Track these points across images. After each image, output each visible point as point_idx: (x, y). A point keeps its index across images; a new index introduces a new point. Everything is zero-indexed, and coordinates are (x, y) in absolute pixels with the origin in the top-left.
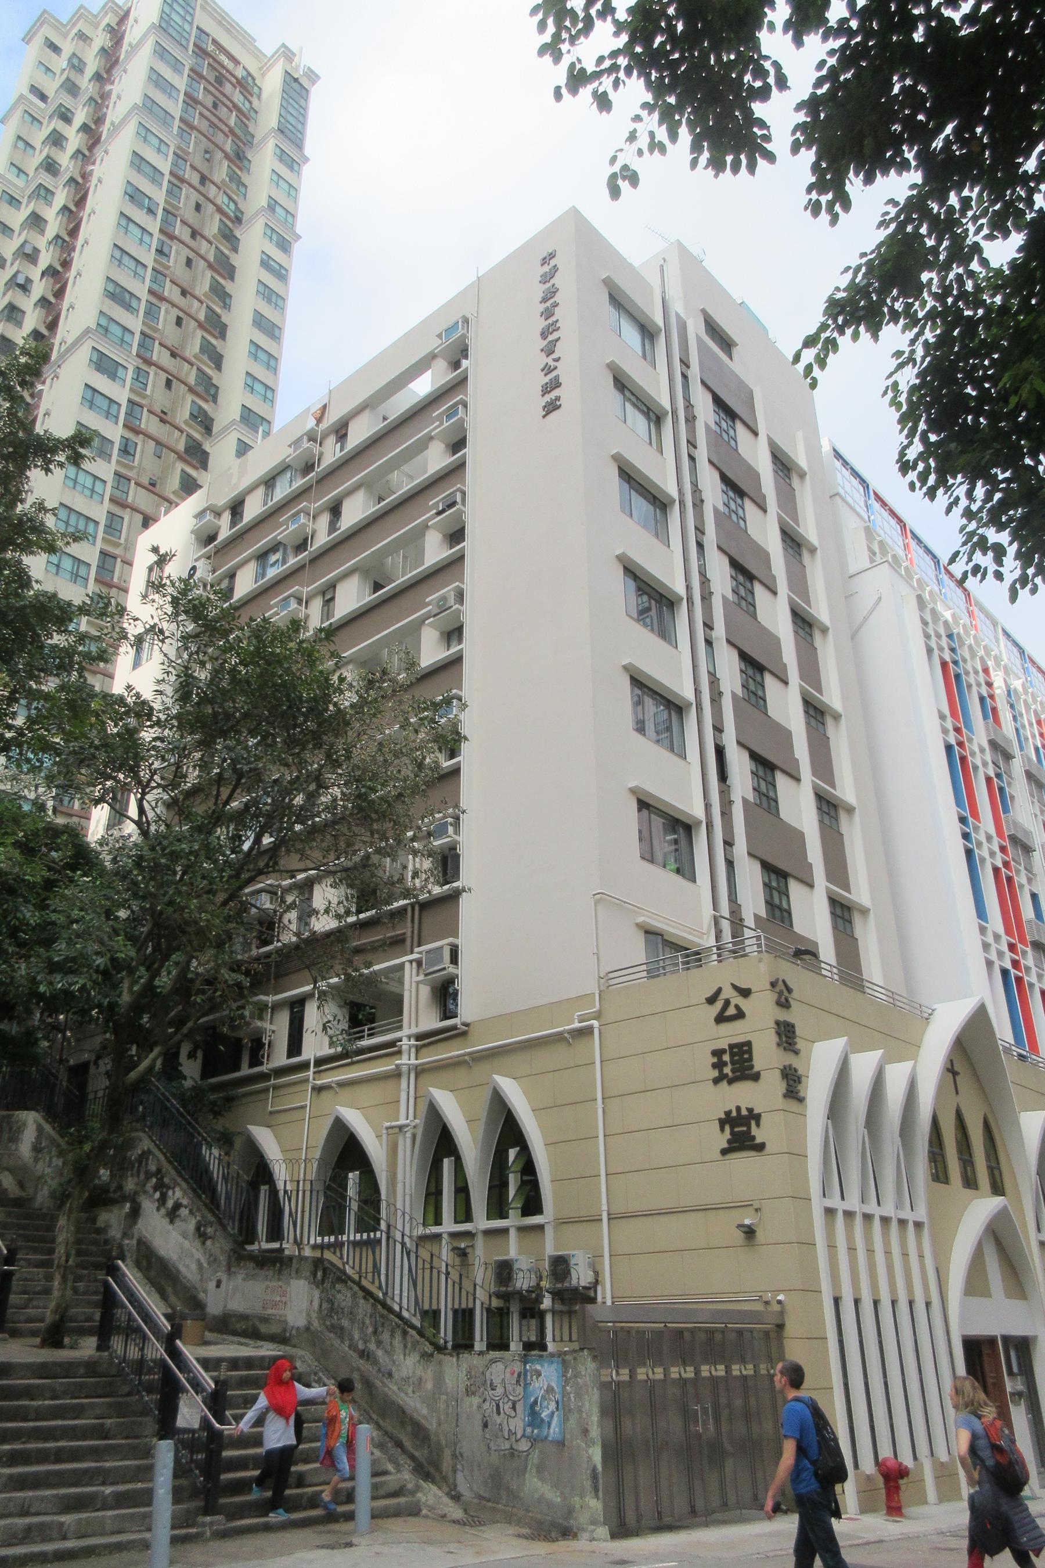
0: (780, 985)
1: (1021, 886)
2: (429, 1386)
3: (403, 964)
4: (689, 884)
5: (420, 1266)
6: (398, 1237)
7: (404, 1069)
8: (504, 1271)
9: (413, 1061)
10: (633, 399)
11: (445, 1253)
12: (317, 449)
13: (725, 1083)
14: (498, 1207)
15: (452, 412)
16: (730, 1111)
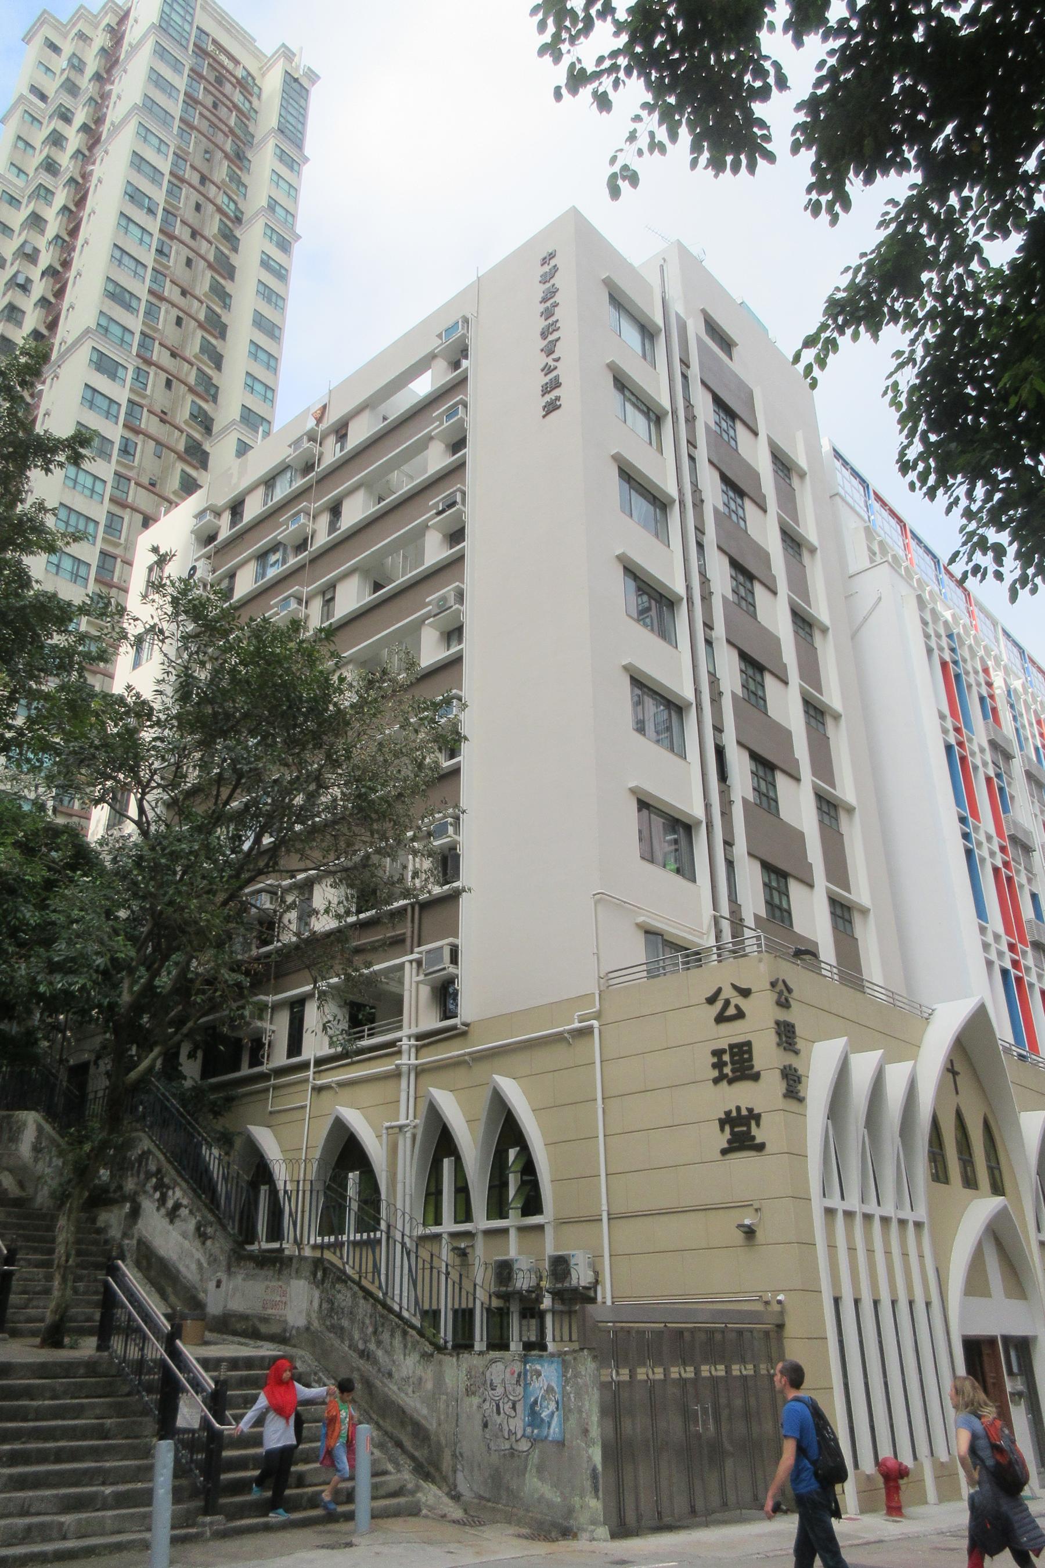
0: (780, 985)
1: (1021, 886)
2: (429, 1386)
3: (403, 964)
4: (689, 884)
5: (420, 1266)
6: (398, 1237)
7: (404, 1069)
8: (504, 1271)
9: (413, 1061)
10: (633, 399)
11: (445, 1253)
12: (317, 449)
13: (725, 1083)
14: (498, 1207)
15: (452, 412)
16: (730, 1111)
